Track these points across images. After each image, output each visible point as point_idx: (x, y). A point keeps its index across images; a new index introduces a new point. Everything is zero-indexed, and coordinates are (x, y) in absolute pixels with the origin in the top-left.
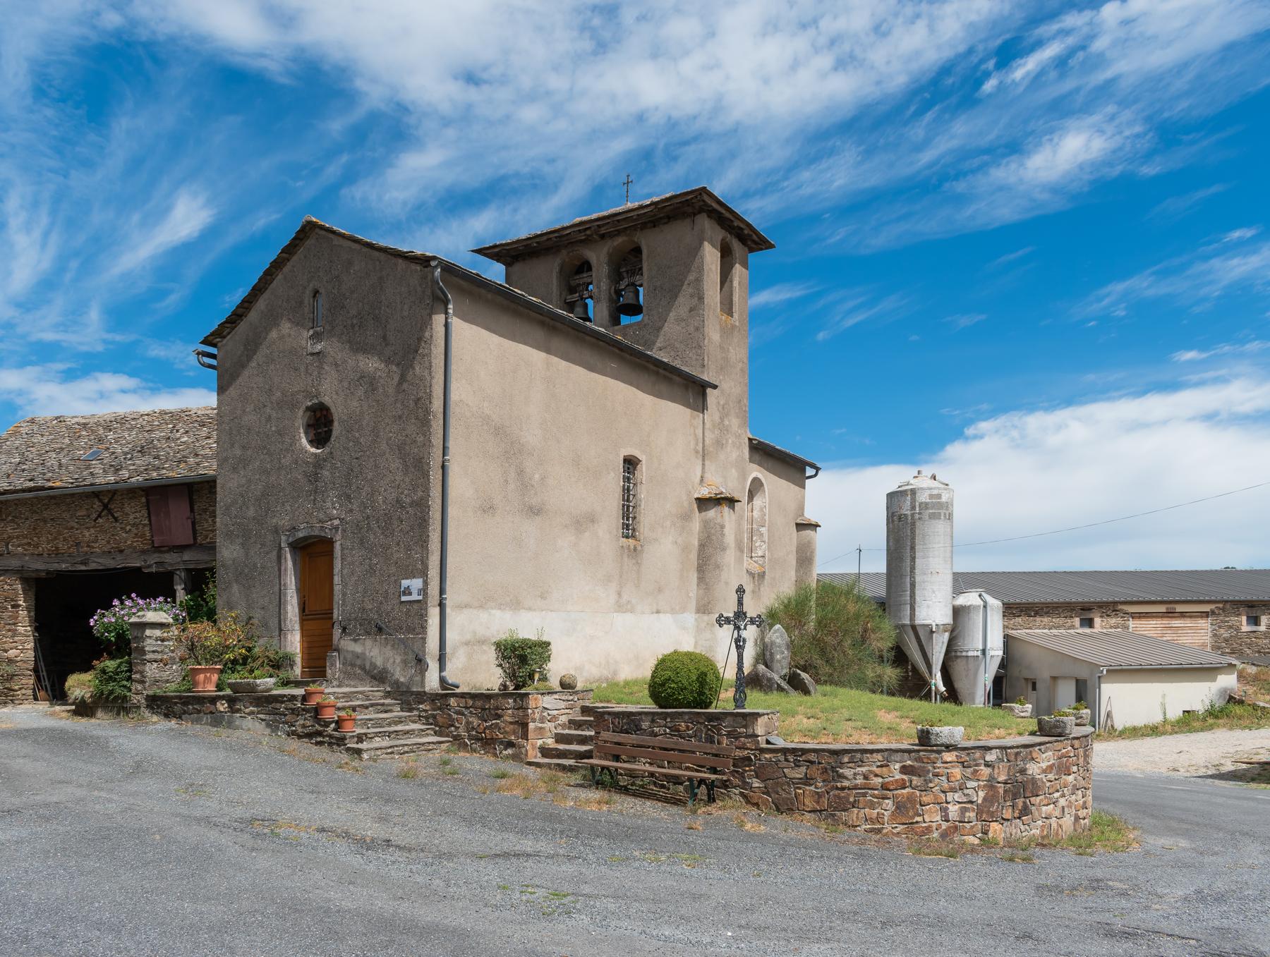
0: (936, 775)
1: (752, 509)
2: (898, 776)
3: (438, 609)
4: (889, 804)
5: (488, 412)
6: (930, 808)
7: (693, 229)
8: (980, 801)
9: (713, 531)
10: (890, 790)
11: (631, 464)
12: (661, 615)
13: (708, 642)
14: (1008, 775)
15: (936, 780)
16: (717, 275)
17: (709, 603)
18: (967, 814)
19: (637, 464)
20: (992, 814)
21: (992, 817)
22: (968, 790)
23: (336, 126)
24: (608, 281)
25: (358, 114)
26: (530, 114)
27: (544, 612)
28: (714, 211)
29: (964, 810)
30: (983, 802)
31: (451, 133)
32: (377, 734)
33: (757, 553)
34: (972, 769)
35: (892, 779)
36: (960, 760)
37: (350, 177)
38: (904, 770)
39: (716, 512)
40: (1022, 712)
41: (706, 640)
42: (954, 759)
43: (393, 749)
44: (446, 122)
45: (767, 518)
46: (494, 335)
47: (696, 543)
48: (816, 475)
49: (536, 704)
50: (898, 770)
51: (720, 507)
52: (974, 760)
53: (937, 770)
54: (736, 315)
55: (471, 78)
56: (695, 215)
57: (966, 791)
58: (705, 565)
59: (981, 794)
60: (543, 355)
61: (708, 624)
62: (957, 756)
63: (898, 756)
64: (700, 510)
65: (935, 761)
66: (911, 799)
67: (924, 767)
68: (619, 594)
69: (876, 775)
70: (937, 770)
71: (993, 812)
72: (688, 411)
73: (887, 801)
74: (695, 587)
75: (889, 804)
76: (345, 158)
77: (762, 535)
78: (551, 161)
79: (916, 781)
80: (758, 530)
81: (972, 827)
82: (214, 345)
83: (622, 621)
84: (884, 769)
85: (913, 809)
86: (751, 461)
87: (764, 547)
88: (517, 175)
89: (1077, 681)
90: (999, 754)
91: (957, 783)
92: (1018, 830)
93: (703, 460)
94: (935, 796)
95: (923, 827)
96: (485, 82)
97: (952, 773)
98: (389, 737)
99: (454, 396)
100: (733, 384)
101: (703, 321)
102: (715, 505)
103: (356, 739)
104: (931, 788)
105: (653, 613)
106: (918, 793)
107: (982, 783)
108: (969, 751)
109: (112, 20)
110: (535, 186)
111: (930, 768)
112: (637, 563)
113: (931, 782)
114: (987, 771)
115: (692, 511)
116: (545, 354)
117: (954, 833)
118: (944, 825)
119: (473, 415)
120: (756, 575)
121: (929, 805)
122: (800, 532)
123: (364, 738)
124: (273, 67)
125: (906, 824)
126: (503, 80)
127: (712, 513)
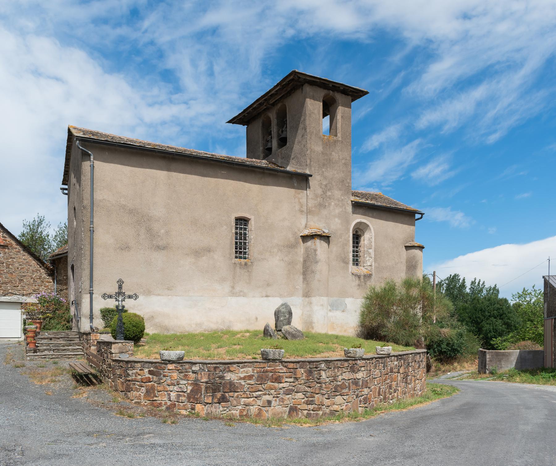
0: (164, 376)
1: (364, 240)
2: (148, 375)
3: (89, 295)
4: (143, 389)
6: (162, 393)
7: (302, 93)
8: (189, 392)
9: (310, 253)
10: (144, 383)
11: (242, 222)
12: (270, 298)
13: (308, 312)
14: (209, 378)
15: (164, 379)
16: (319, 114)
17: (309, 291)
18: (181, 398)
19: (249, 221)
20: (197, 399)
21: (197, 401)
22: (181, 385)
23: (397, 58)
24: (277, 127)
25: (407, 50)
26: (502, 28)
27: (170, 296)
29: (179, 396)
30: (190, 392)
31: (457, 48)
32: (45, 350)
34: (184, 374)
35: (144, 377)
36: (176, 369)
37: (406, 82)
38: (150, 372)
40: (382, 351)
41: (307, 311)
42: (174, 368)
43: (45, 356)
44: (454, 43)
45: (373, 244)
46: (127, 167)
47: (302, 260)
48: (421, 218)
50: (148, 372)
52: (186, 369)
53: (165, 374)
54: (339, 135)
55: (466, 16)
56: (303, 85)
57: (180, 386)
58: (306, 271)
59: (190, 388)
60: (165, 173)
61: (308, 303)
62: (175, 366)
63: (147, 365)
64: (304, 242)
65: (164, 369)
66: (153, 388)
67: (158, 371)
68: (233, 287)
69: (139, 375)
70: (165, 374)
71: (197, 398)
72: (292, 191)
73: (142, 388)
74: (301, 283)
75: (143, 389)
76: (403, 74)
77: (370, 254)
78: (518, 50)
79: (155, 378)
80: (367, 251)
81: (184, 405)
82: (66, 185)
83: (233, 301)
84: (142, 371)
85: (153, 393)
86: (354, 213)
88: (498, 63)
90: (201, 367)
91: (175, 381)
92: (218, 409)
93: (307, 216)
94: (164, 387)
95: (158, 403)
96: (474, 16)
97: (172, 375)
98: (53, 351)
100: (336, 172)
101: (306, 141)
102: (311, 239)
103: (33, 351)
104: (162, 383)
105: (263, 297)
106: (156, 385)
107: (190, 382)
108: (182, 364)
109: (291, 32)
110: (509, 67)
111: (162, 372)
112: (248, 271)
113: (161, 379)
114: (194, 375)
115: (297, 243)
116: (166, 172)
117: (174, 407)
118: (169, 403)
120: (362, 277)
121: (162, 391)
123: (38, 351)
124: (362, 36)
125: (150, 401)
126: (485, 13)
127: (310, 243)
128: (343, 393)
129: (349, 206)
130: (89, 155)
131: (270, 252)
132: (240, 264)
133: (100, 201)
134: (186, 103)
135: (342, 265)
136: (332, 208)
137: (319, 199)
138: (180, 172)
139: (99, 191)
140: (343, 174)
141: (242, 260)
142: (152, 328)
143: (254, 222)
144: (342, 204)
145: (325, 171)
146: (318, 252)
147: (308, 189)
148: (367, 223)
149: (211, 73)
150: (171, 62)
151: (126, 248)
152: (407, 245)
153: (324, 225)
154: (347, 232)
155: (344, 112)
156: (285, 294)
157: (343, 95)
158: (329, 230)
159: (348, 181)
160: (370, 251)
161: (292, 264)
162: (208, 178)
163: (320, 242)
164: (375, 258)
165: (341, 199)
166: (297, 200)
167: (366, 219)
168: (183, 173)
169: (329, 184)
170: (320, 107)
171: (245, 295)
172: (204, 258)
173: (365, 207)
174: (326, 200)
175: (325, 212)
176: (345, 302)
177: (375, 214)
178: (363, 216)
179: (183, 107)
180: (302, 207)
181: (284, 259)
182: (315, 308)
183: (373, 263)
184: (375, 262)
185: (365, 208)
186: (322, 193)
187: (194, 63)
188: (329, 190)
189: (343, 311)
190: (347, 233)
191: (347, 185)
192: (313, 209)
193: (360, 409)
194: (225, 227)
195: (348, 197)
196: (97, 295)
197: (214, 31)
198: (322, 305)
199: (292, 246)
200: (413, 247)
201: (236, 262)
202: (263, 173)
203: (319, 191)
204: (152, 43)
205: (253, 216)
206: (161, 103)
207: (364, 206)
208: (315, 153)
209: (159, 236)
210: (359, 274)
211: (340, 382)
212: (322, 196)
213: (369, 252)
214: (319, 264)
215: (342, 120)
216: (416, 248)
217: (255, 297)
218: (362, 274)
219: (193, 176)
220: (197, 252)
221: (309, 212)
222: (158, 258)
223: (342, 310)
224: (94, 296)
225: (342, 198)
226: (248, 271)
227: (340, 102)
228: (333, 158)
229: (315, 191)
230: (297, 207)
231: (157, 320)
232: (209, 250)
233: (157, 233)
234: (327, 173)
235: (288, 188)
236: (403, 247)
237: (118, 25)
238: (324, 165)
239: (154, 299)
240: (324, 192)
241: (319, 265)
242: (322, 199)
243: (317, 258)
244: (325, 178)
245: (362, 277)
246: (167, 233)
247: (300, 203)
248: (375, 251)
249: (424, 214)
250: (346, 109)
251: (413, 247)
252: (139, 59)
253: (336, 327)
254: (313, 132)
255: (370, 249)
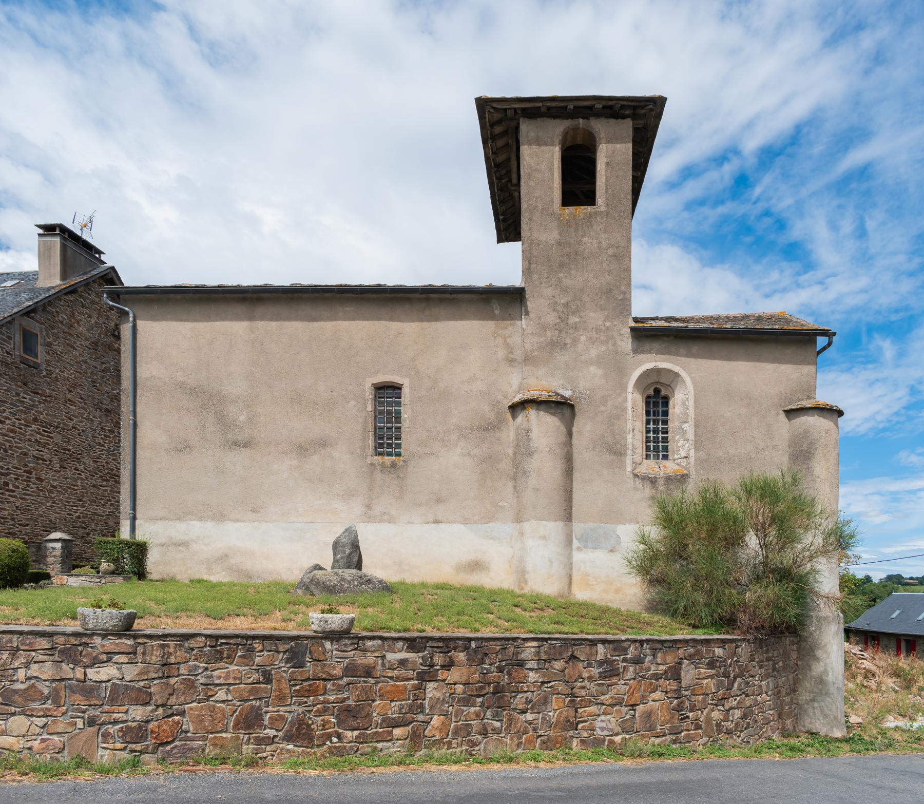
5: (182, 379)
16: (551, 169)
27: (256, 523)
28: (523, 109)
33: (680, 454)
39: (523, 416)
48: (829, 344)
49: (61, 582)
51: (525, 411)
60: (245, 324)
64: (514, 417)
68: (369, 507)
72: (490, 325)
77: (685, 432)
80: (681, 428)
86: (635, 351)
87: (687, 446)
89: (141, 574)
99: (142, 373)
100: (591, 276)
105: (428, 523)
112: (398, 477)
119: (165, 384)
120: (661, 482)
122: (793, 421)
128: (32, 710)
129: (625, 339)
130: (127, 313)
131: (443, 441)
132: (383, 465)
133: (147, 379)
134: (821, 283)
135: (608, 457)
136: (580, 347)
137: (549, 334)
138: (271, 320)
139: (144, 365)
140: (609, 278)
141: (386, 458)
142: (224, 573)
143: (410, 388)
144: (607, 336)
145: (566, 277)
146: (534, 434)
147: (523, 317)
148: (672, 369)
149: (861, 233)
150: (796, 231)
151: (184, 448)
152: (786, 408)
153: (561, 382)
154: (618, 391)
155: (613, 153)
156: (476, 518)
157: (612, 121)
158: (573, 391)
159: (623, 288)
160: (685, 426)
161: (489, 461)
162: (319, 323)
163: (538, 413)
164: (696, 441)
165: (603, 328)
166: (500, 340)
167: (672, 362)
168: (276, 320)
169: (574, 301)
170: (552, 156)
171: (391, 521)
172: (315, 457)
173: (668, 336)
174: (567, 333)
175: (562, 357)
176: (614, 532)
177: (695, 348)
178: (663, 356)
179: (817, 289)
180: (512, 353)
181: (471, 453)
182: (530, 543)
183: (693, 451)
184: (697, 449)
185: (668, 339)
186: (558, 321)
187: (833, 226)
188: (573, 313)
189: (612, 551)
190: (620, 395)
191: (620, 297)
192: (536, 353)
193: (101, 752)
194: (353, 403)
195: (622, 321)
196: (142, 522)
197: (864, 172)
198: (544, 538)
199: (491, 427)
200: (803, 410)
201: (374, 462)
202: (427, 299)
203: (551, 318)
204: (767, 213)
205: (408, 379)
206: (784, 290)
207: (664, 335)
208: (541, 246)
209: (237, 426)
210: (653, 476)
211: (22, 683)
212: (557, 327)
213: (683, 429)
214: (536, 456)
215: (606, 171)
216: (811, 412)
217: (412, 523)
218: (662, 475)
219: (294, 323)
220: (302, 447)
221: (528, 359)
222: (238, 460)
223: (610, 548)
224: (137, 522)
225: (608, 324)
226: (398, 477)
227: (602, 135)
228: (585, 249)
229: (540, 318)
230: (501, 354)
231: (233, 561)
232: (323, 443)
233: (234, 421)
234: (569, 280)
235: (480, 320)
236: (778, 414)
237: (719, 202)
238: (561, 266)
239: (230, 526)
240: (563, 319)
241: (534, 458)
242: (557, 332)
243: (531, 445)
244: (565, 291)
245: (661, 482)
246: (251, 420)
247: (508, 345)
248: (696, 426)
249: (834, 334)
250: (618, 146)
251: (803, 410)
252: (749, 239)
253: (595, 583)
254: (537, 206)
255: (685, 422)
